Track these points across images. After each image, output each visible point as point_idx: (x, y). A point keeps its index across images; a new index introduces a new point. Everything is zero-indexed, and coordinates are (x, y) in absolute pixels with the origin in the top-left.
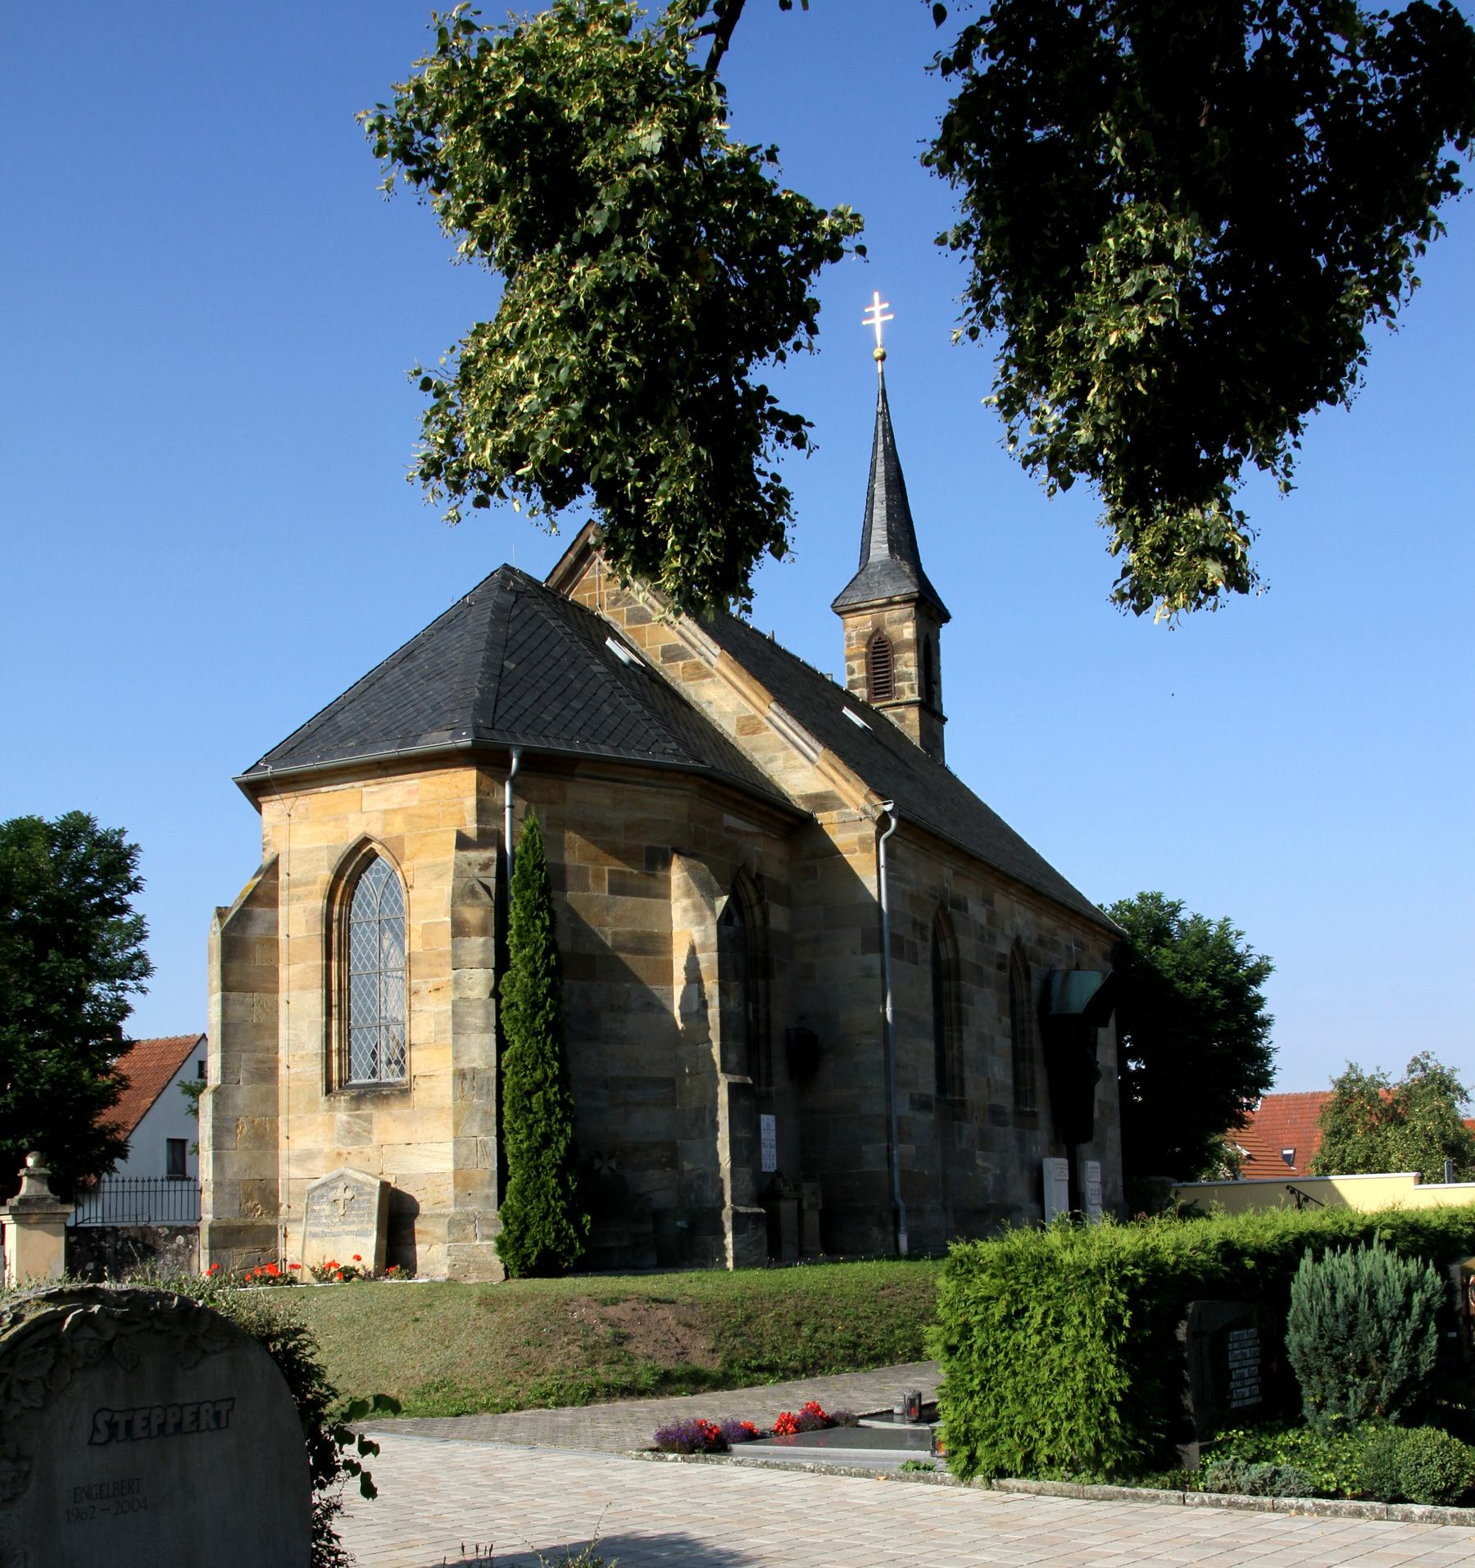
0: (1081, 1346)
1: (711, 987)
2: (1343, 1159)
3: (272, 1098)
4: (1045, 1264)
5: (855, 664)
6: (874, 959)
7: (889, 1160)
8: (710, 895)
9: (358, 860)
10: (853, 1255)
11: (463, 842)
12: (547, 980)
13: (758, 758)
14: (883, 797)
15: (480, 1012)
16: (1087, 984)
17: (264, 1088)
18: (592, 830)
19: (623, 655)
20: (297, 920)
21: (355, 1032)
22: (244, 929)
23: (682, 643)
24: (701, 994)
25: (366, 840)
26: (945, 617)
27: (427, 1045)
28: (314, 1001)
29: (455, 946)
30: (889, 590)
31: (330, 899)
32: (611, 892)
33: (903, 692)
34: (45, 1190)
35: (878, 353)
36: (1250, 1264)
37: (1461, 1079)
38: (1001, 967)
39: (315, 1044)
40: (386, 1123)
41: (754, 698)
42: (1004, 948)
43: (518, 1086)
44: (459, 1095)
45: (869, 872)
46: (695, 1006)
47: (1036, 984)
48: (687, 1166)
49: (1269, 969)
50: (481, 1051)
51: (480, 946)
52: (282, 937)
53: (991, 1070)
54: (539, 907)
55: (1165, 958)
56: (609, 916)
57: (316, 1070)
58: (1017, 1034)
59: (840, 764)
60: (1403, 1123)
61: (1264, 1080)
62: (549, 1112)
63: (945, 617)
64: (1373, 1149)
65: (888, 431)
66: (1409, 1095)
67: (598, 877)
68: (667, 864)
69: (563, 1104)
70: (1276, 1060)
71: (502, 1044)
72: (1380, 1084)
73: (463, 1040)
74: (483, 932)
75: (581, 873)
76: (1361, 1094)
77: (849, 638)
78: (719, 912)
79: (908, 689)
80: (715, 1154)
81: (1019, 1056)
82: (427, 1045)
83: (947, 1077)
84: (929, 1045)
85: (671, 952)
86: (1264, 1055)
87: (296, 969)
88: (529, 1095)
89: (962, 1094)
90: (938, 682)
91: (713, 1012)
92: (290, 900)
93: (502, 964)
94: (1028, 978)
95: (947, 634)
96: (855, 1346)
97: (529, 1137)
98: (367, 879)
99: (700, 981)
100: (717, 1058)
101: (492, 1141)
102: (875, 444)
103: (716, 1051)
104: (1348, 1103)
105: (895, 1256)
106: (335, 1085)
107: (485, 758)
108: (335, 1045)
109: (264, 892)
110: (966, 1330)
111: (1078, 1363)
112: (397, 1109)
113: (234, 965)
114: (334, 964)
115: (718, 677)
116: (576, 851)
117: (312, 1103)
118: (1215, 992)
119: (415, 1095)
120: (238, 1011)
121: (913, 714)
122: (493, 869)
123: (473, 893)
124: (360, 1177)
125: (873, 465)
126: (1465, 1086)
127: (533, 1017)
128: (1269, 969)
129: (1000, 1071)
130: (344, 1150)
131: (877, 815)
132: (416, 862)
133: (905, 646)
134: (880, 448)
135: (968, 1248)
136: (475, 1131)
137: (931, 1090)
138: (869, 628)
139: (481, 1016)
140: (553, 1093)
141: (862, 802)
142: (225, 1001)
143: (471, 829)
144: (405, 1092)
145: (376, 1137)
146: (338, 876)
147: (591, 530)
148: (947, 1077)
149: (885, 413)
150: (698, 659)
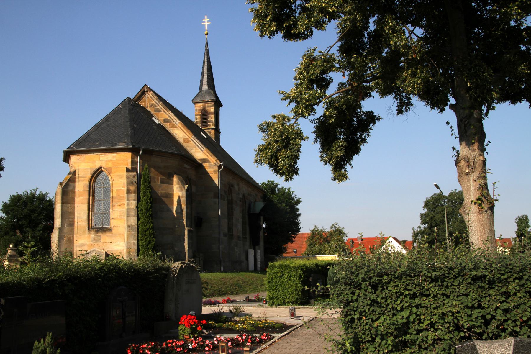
0: (294, 281)
1: (184, 206)
2: (313, 252)
3: (73, 230)
4: (287, 267)
5: (198, 117)
6: (217, 200)
7: (219, 248)
8: (184, 185)
9: (97, 173)
10: (210, 271)
11: (128, 170)
12: (150, 205)
13: (188, 149)
14: (220, 161)
15: (134, 211)
16: (260, 205)
17: (71, 228)
18: (157, 168)
19: (157, 122)
20: (81, 187)
21: (96, 215)
22: (67, 188)
23: (169, 118)
24: (181, 208)
25: (101, 168)
26: (221, 105)
27: (117, 219)
28: (85, 207)
29: (127, 195)
30: (208, 98)
31: (90, 181)
32: (161, 183)
33: (210, 125)
34: (15, 253)
35: (206, 32)
36: (320, 268)
37: (345, 231)
38: (240, 201)
39: (85, 217)
40: (105, 238)
41: (188, 134)
42: (241, 196)
43: (143, 229)
44: (128, 231)
45: (216, 179)
46: (179, 211)
47: (247, 205)
48: (176, 249)
49: (300, 201)
50: (133, 220)
51: (133, 196)
52: (76, 190)
53: (238, 228)
54: (148, 187)
55: (275, 198)
56: (160, 189)
57: (86, 224)
58: (243, 218)
59: (209, 152)
60: (329, 242)
61: (298, 230)
62: (150, 236)
63: (221, 105)
64: (321, 250)
65: (208, 54)
66: (331, 234)
67: (158, 179)
68: (173, 177)
69: (153, 234)
70: (301, 225)
71: (138, 219)
72: (323, 232)
73: (129, 218)
74: (135, 192)
75: (154, 178)
76: (318, 234)
77: (196, 110)
78: (186, 188)
79: (212, 125)
80: (184, 246)
81: (244, 223)
82: (117, 219)
83: (230, 229)
84: (227, 221)
85: (173, 197)
86: (298, 224)
87: (80, 198)
88: (145, 231)
89: (232, 232)
90: (219, 123)
91: (184, 212)
92: (79, 181)
93: (139, 200)
94: (245, 204)
95: (221, 109)
96: (220, 291)
97: (146, 241)
98: (100, 177)
99: (181, 205)
100: (185, 224)
101: (136, 242)
102: (205, 57)
103: (185, 222)
104: (314, 237)
105: (221, 272)
106: (90, 228)
107: (134, 151)
108: (90, 218)
109: (72, 178)
110: (272, 278)
111: (293, 285)
112: (108, 234)
113: (65, 197)
114: (91, 198)
115: (178, 128)
116: (153, 173)
117: (84, 232)
118: (287, 207)
119: (113, 231)
120: (65, 209)
121: (213, 132)
122: (136, 177)
123: (132, 183)
124: (99, 250)
125: (204, 63)
126: (346, 233)
127: (147, 213)
128: (300, 201)
129: (240, 227)
130: (93, 244)
131: (218, 165)
132: (115, 174)
133: (211, 113)
134: (206, 59)
135: (272, 264)
136: (132, 240)
137: (227, 232)
138: (202, 108)
139: (133, 212)
140: (151, 231)
141: (215, 162)
142: (62, 206)
143: (130, 167)
144: (110, 230)
145: (102, 241)
146: (93, 176)
147: (146, 87)
148: (230, 229)
149: (207, 49)
150: (173, 123)
